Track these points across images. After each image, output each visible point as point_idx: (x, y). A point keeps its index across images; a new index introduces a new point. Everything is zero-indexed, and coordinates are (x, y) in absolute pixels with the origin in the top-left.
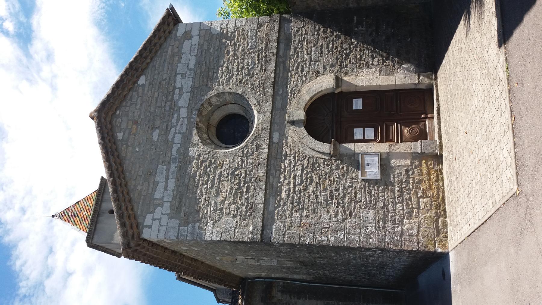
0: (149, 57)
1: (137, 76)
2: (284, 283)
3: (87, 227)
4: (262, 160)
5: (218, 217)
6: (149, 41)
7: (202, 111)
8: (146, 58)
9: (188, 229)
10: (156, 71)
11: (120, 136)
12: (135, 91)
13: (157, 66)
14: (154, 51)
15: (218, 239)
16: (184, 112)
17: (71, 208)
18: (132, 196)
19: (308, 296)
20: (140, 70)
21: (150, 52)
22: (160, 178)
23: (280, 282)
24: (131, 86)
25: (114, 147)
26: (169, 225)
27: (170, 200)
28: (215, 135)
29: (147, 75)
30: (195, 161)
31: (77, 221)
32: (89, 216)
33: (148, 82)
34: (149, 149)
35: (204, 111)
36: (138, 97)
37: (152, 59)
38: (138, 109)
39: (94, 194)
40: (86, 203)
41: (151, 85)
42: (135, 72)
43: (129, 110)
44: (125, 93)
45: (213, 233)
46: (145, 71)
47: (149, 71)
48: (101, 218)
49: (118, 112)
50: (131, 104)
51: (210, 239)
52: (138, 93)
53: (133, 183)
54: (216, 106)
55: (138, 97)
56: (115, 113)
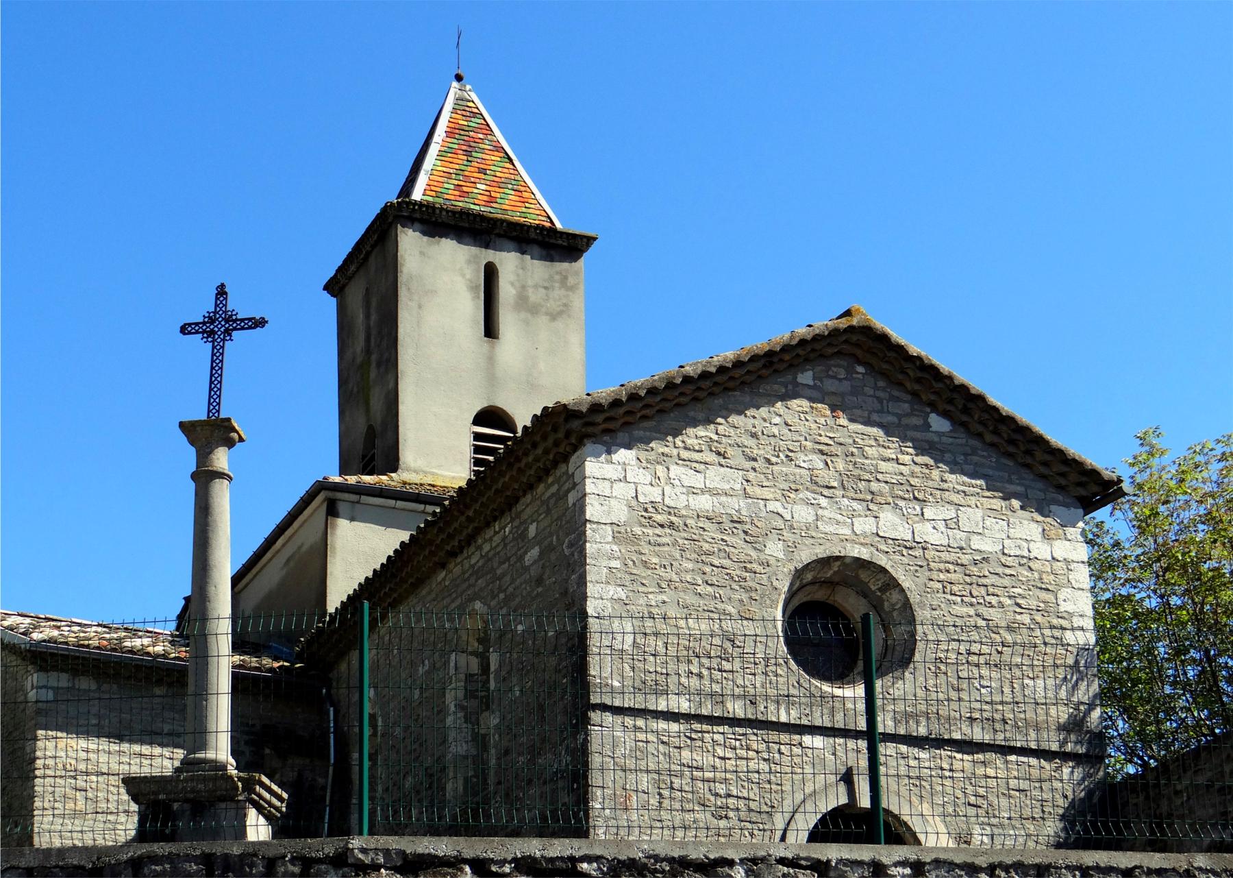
0: (995, 439)
1: (949, 411)
2: (324, 788)
3: (439, 195)
4: (762, 709)
5: (636, 611)
6: (1040, 441)
7: (869, 569)
8: (996, 432)
9: (608, 543)
10: (962, 457)
12: (913, 409)
13: (975, 458)
14: (1011, 449)
15: (590, 611)
16: (864, 525)
17: (489, 137)
18: (672, 415)
20: (965, 418)
21: (1012, 442)
22: (715, 477)
23: (326, 777)
24: (924, 397)
25: (782, 366)
26: (613, 502)
27: (667, 501)
28: (808, 598)
29: (952, 434)
30: (754, 554)
31: (455, 161)
32: (472, 201)
33: (936, 439)
34: (777, 449)
35: (869, 572)
36: (900, 417)
37: (992, 445)
38: (869, 418)
39: (538, 212)
40: (510, 186)
41: (927, 447)
42: (960, 407)
43: (865, 395)
44: (908, 385)
45: (601, 601)
46: (962, 430)
47: (962, 438)
49: (861, 369)
50: (880, 400)
51: (589, 594)
52: (907, 415)
54: (881, 601)
55: (900, 417)
56: (860, 363)
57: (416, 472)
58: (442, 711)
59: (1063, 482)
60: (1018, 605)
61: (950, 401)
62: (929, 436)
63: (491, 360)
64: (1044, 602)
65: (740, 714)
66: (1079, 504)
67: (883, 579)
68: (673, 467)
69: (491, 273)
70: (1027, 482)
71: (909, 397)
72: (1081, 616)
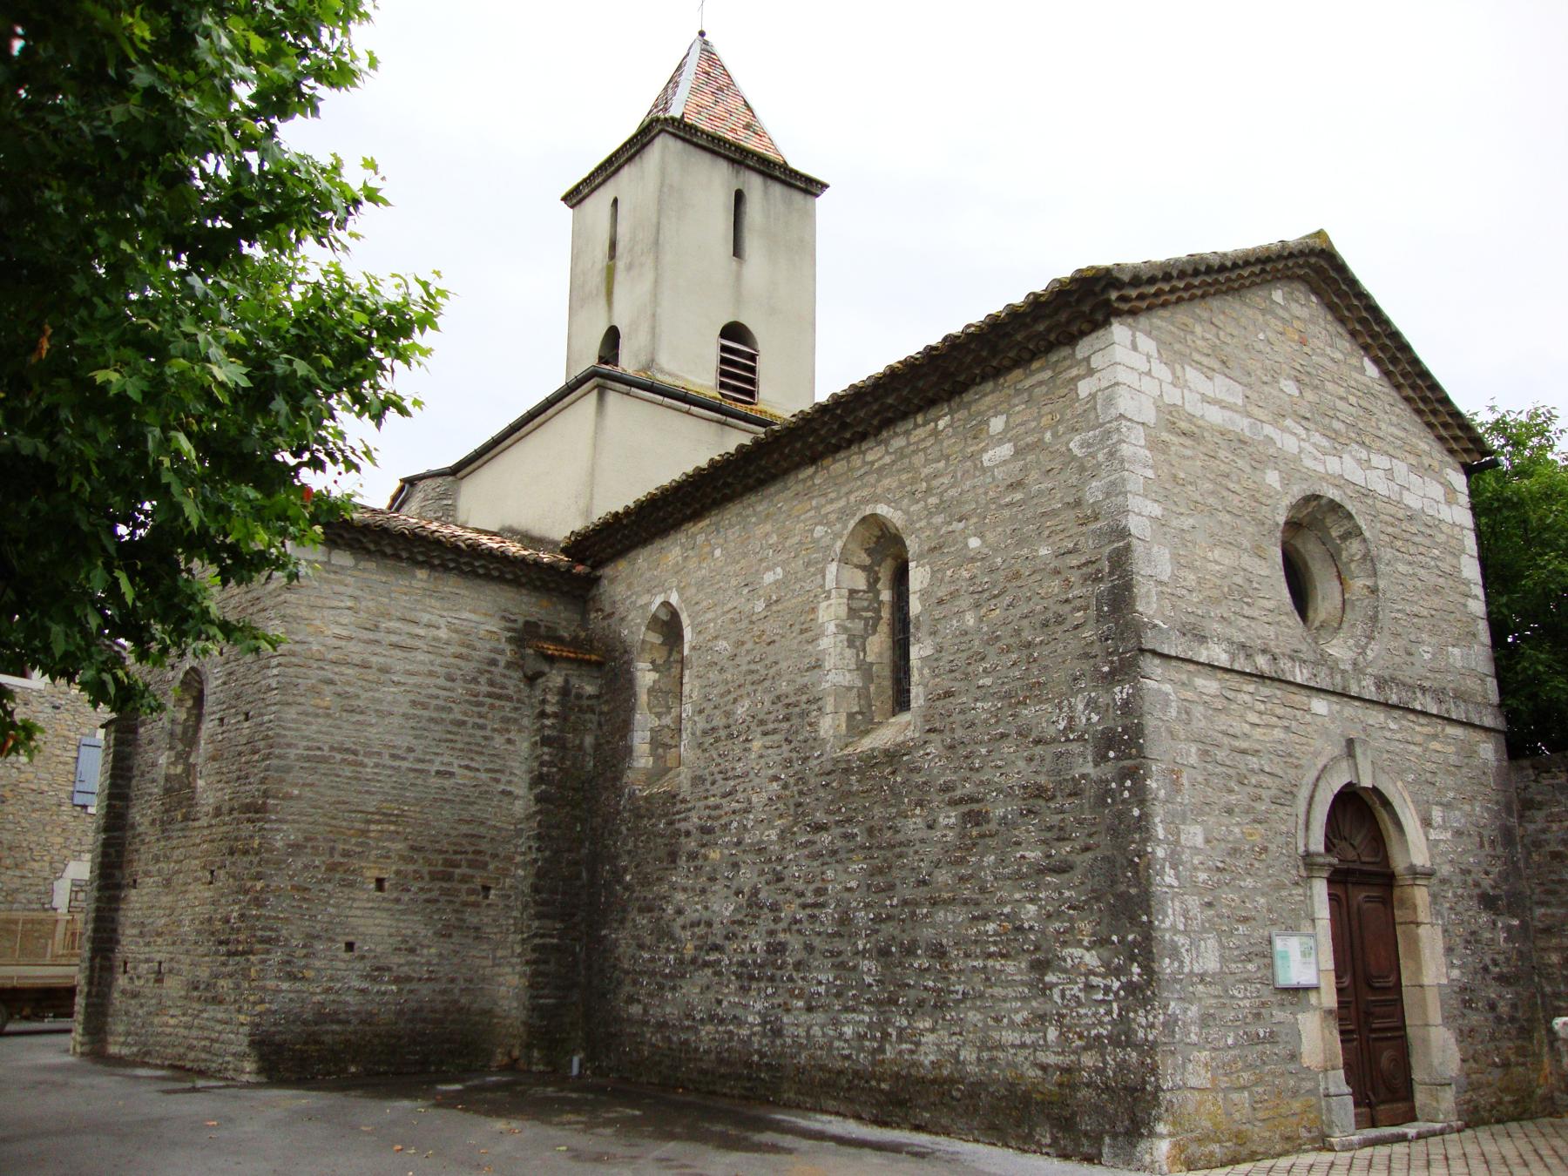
11: (1278, 296)
19: (555, 770)
21: (1424, 400)
22: (1220, 387)
26: (1143, 397)
48: (723, 167)
53: (1205, 315)
54: (1339, 550)
57: (670, 375)
58: (809, 631)
63: (738, 277)
67: (1347, 525)
68: (1188, 368)
69: (739, 197)
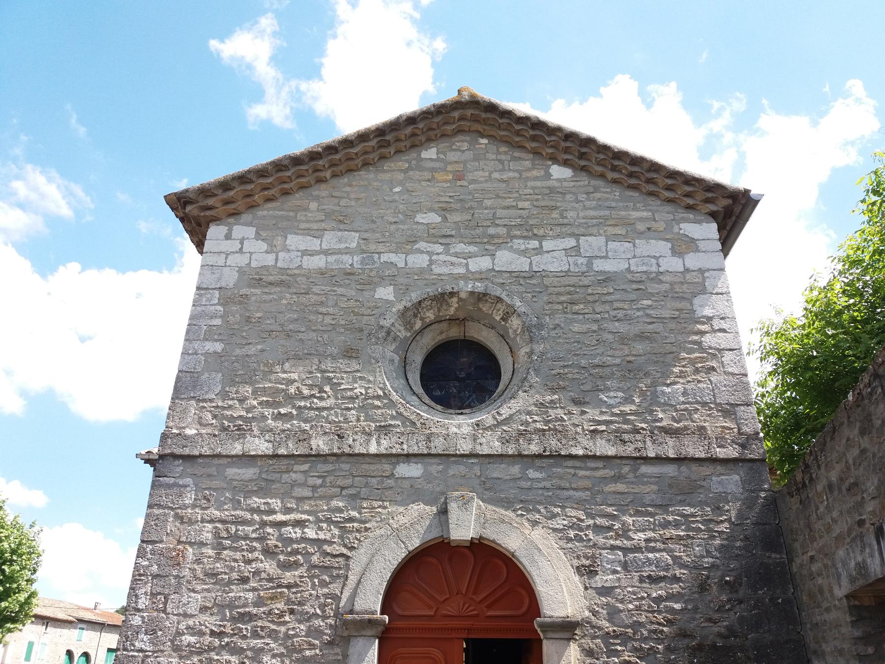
0: (616, 175)
10: (584, 196)
13: (598, 195)
16: (482, 263)
33: (557, 184)
37: (615, 181)
46: (584, 174)
49: (484, 141)
52: (529, 170)
54: (506, 329)
59: (690, 201)
60: (648, 315)
61: (566, 150)
62: (549, 183)
64: (677, 310)
65: (325, 449)
66: (712, 219)
70: (654, 208)
71: (531, 156)
72: (722, 318)
